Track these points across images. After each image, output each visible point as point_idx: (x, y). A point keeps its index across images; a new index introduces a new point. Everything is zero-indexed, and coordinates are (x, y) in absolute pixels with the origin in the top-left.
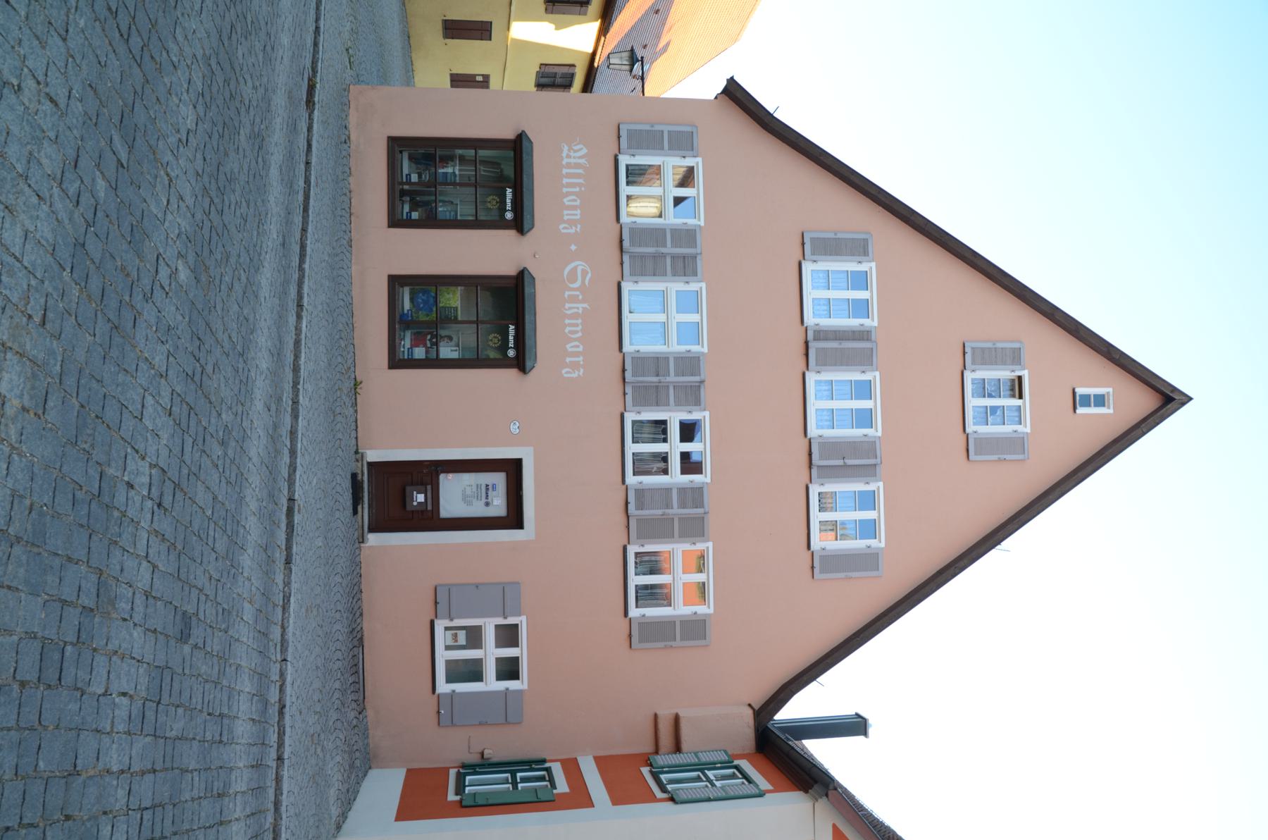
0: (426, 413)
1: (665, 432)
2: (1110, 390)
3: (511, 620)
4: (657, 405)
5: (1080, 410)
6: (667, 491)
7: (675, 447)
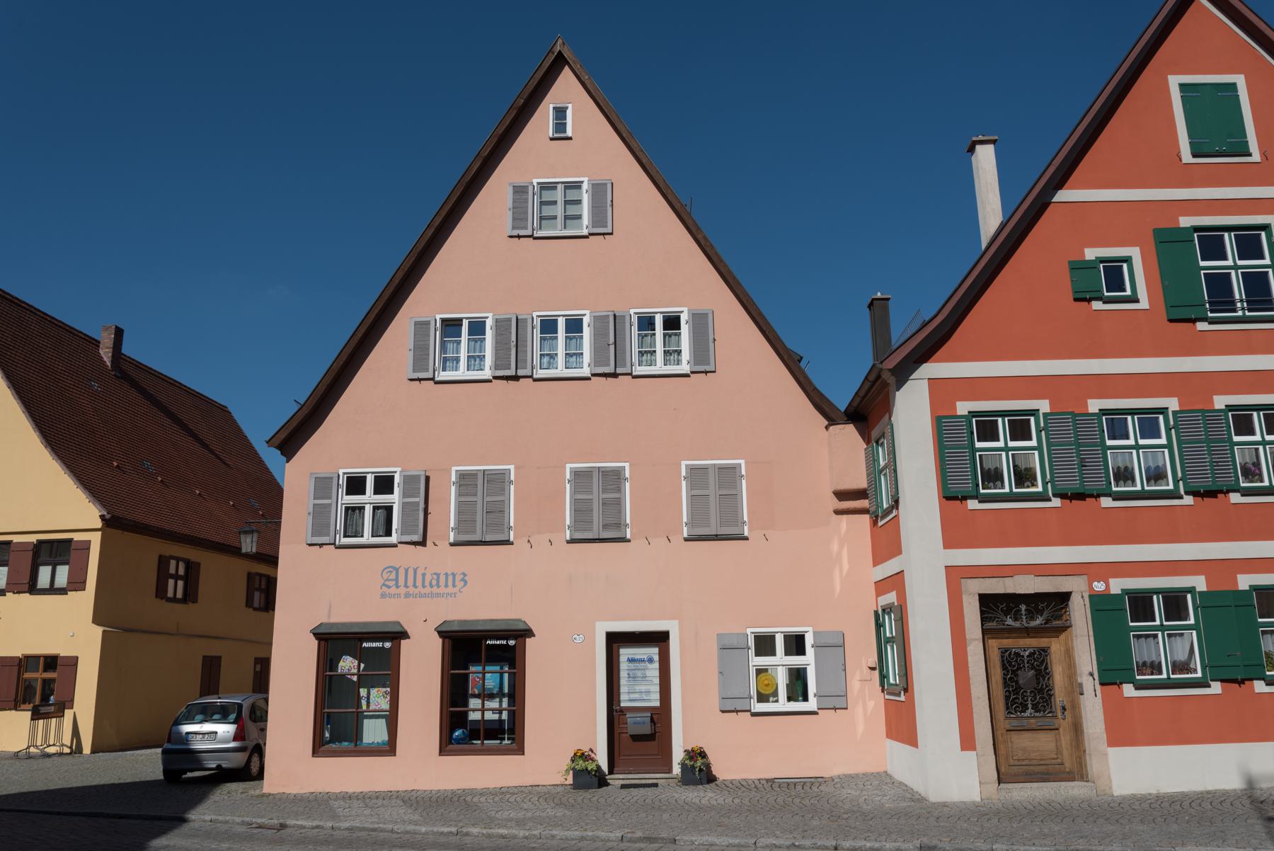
0: (565, 714)
1: (354, 509)
2: (1256, 157)
3: (751, 643)
4: (502, 511)
5: (569, 133)
6: (404, 506)
7: (369, 498)
